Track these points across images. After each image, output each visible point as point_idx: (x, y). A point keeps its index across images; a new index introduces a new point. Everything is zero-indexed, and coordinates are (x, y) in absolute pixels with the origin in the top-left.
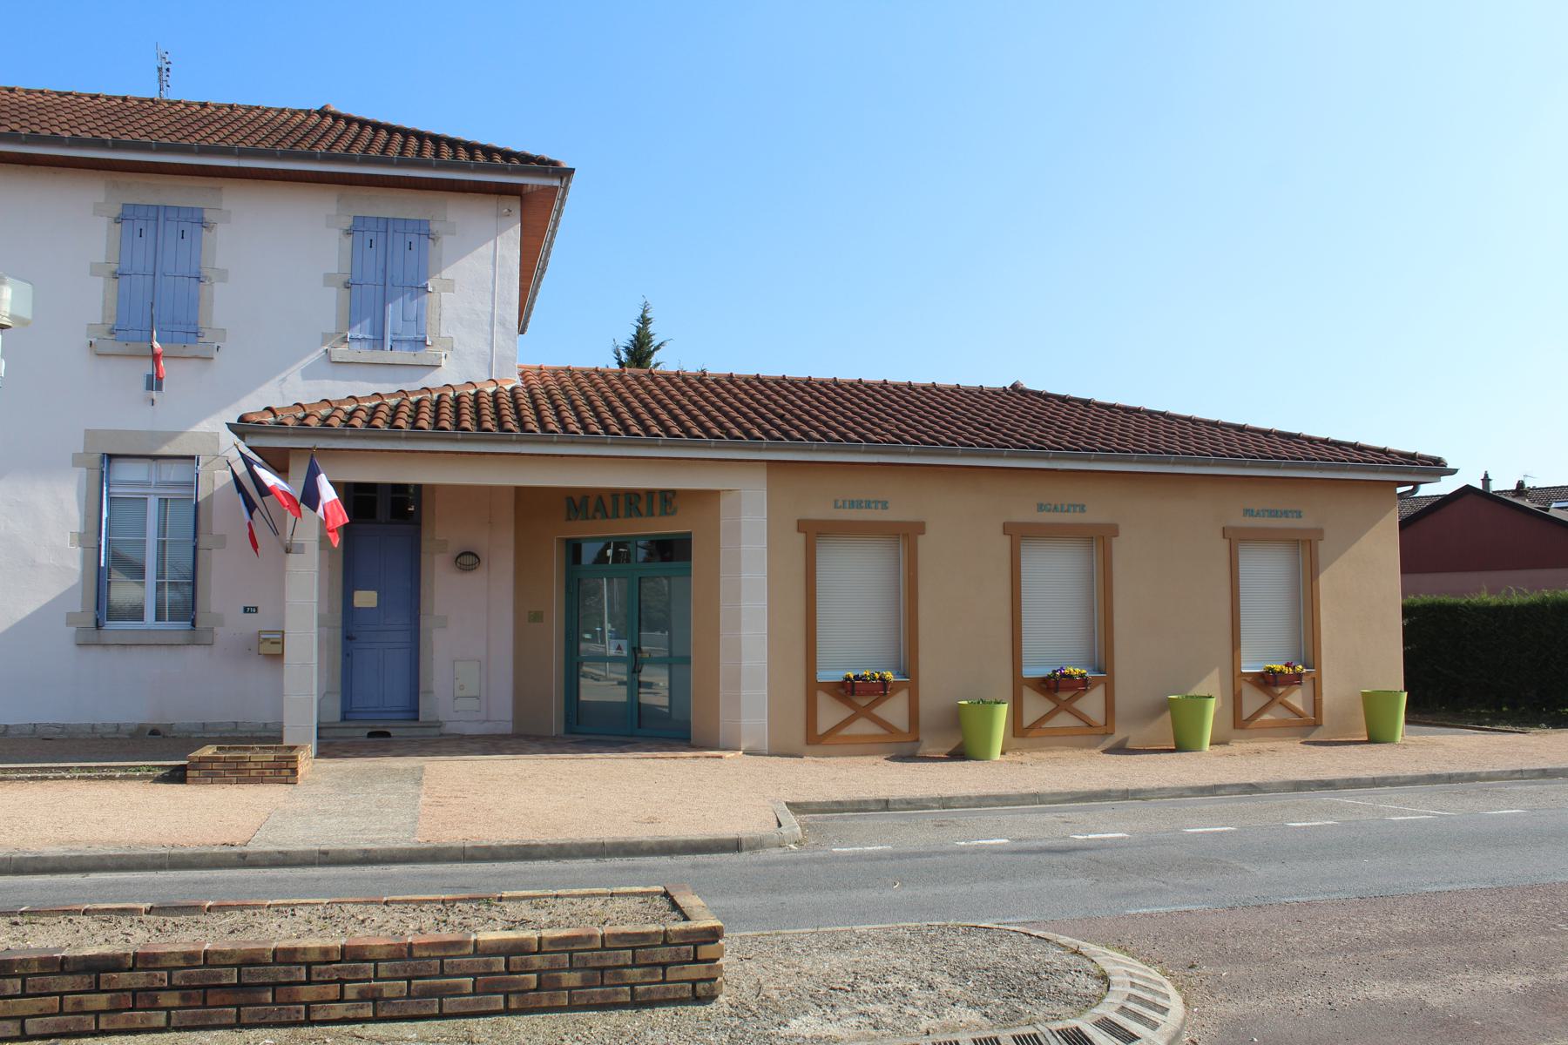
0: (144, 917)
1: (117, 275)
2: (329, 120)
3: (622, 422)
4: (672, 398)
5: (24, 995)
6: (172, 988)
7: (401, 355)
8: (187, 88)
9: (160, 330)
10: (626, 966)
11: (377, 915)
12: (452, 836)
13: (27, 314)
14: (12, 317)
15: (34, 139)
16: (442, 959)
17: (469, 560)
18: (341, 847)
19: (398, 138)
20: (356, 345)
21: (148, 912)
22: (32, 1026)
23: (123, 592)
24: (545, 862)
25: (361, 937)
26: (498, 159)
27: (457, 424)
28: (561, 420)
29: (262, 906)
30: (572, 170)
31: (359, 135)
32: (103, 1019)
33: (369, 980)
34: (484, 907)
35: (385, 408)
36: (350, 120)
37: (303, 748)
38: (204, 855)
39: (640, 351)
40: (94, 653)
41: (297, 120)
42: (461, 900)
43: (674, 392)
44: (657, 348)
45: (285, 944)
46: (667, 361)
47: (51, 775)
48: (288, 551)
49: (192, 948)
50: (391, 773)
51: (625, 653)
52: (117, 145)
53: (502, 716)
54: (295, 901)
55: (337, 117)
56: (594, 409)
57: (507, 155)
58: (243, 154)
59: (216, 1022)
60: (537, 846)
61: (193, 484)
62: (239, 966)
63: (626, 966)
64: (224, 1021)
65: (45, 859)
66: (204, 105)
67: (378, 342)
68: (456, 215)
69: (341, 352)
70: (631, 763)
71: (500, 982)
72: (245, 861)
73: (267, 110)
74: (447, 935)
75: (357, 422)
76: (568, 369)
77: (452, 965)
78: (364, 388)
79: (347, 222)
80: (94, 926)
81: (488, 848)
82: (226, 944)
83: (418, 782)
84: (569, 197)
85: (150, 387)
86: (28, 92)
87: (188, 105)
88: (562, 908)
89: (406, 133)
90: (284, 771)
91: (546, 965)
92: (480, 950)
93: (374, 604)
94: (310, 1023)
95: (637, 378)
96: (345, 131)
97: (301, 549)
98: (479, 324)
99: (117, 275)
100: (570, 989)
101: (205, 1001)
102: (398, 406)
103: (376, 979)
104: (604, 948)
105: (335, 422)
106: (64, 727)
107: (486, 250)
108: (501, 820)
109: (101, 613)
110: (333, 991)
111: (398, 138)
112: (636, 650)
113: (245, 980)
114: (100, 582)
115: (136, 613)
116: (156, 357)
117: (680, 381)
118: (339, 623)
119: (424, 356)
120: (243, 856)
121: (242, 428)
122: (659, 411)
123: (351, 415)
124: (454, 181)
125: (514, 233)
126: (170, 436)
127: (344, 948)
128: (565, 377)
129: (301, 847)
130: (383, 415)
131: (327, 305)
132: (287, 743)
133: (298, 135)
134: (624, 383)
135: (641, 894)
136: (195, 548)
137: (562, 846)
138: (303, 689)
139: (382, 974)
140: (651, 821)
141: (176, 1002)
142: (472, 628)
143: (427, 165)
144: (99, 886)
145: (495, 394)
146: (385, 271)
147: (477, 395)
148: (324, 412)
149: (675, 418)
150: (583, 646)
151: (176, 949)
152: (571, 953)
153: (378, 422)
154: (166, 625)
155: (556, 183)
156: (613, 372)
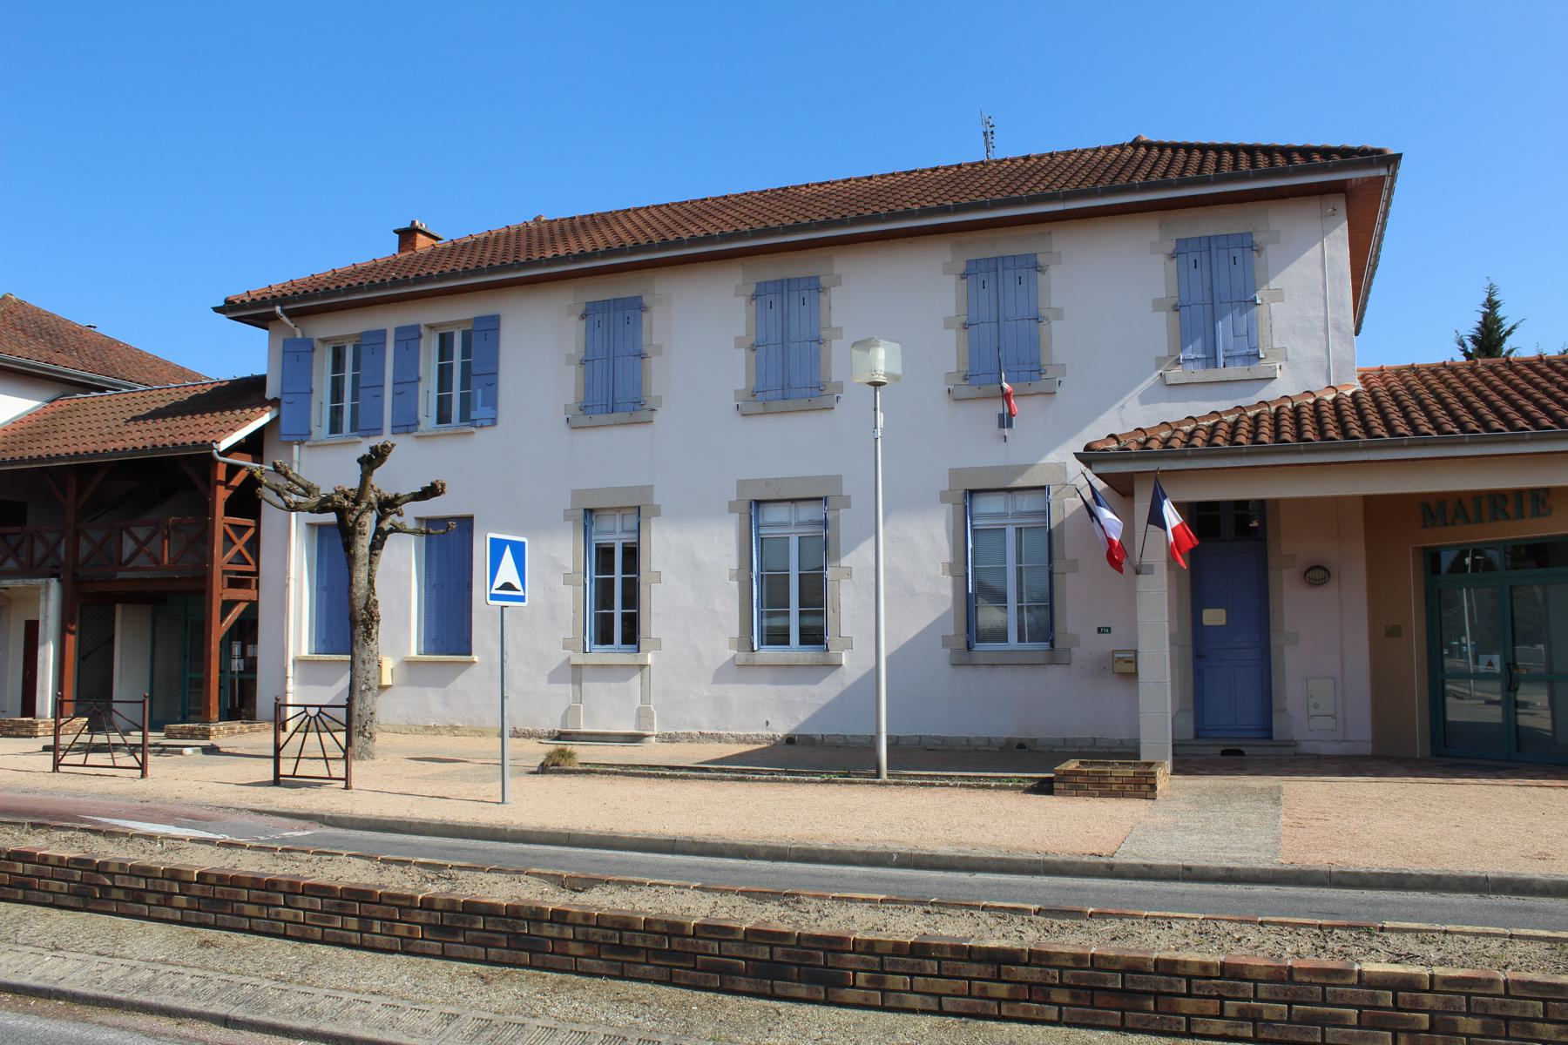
0: (1033, 917)
1: (966, 326)
2: (1143, 151)
3: (1479, 418)
4: (1537, 386)
5: (940, 976)
6: (1062, 986)
7: (1235, 371)
8: (1009, 147)
9: (1007, 372)
10: (1536, 1020)
11: (1253, 935)
12: (1317, 860)
13: (898, 371)
14: (886, 375)
15: (892, 216)
16: (1324, 986)
17: (1317, 574)
18: (1204, 864)
19: (1212, 155)
20: (1190, 366)
21: (1037, 913)
22: (947, 1003)
23: (989, 616)
24: (1419, 894)
25: (1239, 955)
26: (1317, 158)
27: (1299, 435)
28: (1410, 422)
29: (1139, 917)
30: (1400, 156)
31: (1172, 160)
32: (1004, 1006)
33: (1249, 1000)
34: (1365, 937)
35: (1224, 426)
36: (1162, 147)
37: (1160, 764)
38: (1074, 863)
39: (1489, 337)
40: (968, 671)
41: (1113, 155)
42: (1339, 927)
43: (1539, 380)
44: (1509, 333)
45: (1165, 955)
46: (1522, 345)
47: (728, 775)
48: (1138, 572)
49: (1080, 951)
50: (1251, 792)
51: (1497, 669)
52: (959, 209)
53: (1361, 734)
54: (1171, 914)
55: (1149, 146)
56: (1446, 406)
57: (1326, 152)
58: (1068, 196)
59: (1103, 1022)
60: (1410, 875)
61: (1045, 513)
62: (1123, 972)
63: (1536, 1020)
64: (1110, 1023)
65: (939, 857)
66: (1027, 158)
67: (1211, 360)
68: (1279, 223)
69: (1176, 374)
70: (1512, 790)
71: (1388, 1018)
72: (1112, 871)
73: (1083, 152)
74: (1326, 961)
75: (1198, 442)
76: (1412, 367)
77: (1335, 994)
78: (1201, 408)
79: (1171, 247)
80: (991, 921)
81: (1357, 874)
82: (1111, 950)
83: (1276, 801)
84: (1397, 185)
85: (1001, 425)
86: (883, 177)
87: (1013, 161)
88: (1452, 945)
89: (1219, 149)
90: (1143, 787)
91: (1439, 1006)
92: (1364, 980)
93: (1223, 622)
94: (1190, 1035)
95: (1492, 369)
96: (1146, 157)
97: (1150, 570)
98: (1315, 329)
99: (966, 326)
100: (1468, 1036)
101: (1092, 1001)
102: (1237, 422)
103: (1256, 999)
104: (1507, 995)
105: (1176, 443)
106: (944, 739)
107: (1313, 253)
108: (1368, 845)
109: (970, 637)
110: (1213, 1006)
111: (1212, 155)
112: (1510, 666)
113: (1129, 986)
114: (969, 605)
115: (1000, 635)
116: (1006, 397)
117: (1541, 366)
118: (1189, 641)
119: (1258, 370)
120: (1110, 866)
121: (1089, 456)
122: (1523, 402)
123: (1191, 435)
124: (1273, 189)
125: (1341, 232)
126: (1022, 469)
127: (1223, 964)
128: (1410, 376)
129: (1164, 862)
130: (1222, 433)
131: (1157, 329)
132: (1143, 760)
133: (1115, 170)
134: (1478, 375)
135: (1547, 939)
136: (1051, 574)
137: (1438, 877)
138: (1157, 706)
139: (1262, 995)
140: (1543, 857)
141: (1067, 1000)
142: (1324, 647)
143: (1245, 177)
144: (985, 885)
145: (1335, 401)
146: (1211, 289)
147: (1316, 404)
148: (1164, 434)
149: (1543, 408)
150: (1448, 662)
151: (1066, 950)
152: (1468, 996)
153: (1219, 440)
154: (1027, 646)
155: (1383, 172)
156: (1463, 365)
